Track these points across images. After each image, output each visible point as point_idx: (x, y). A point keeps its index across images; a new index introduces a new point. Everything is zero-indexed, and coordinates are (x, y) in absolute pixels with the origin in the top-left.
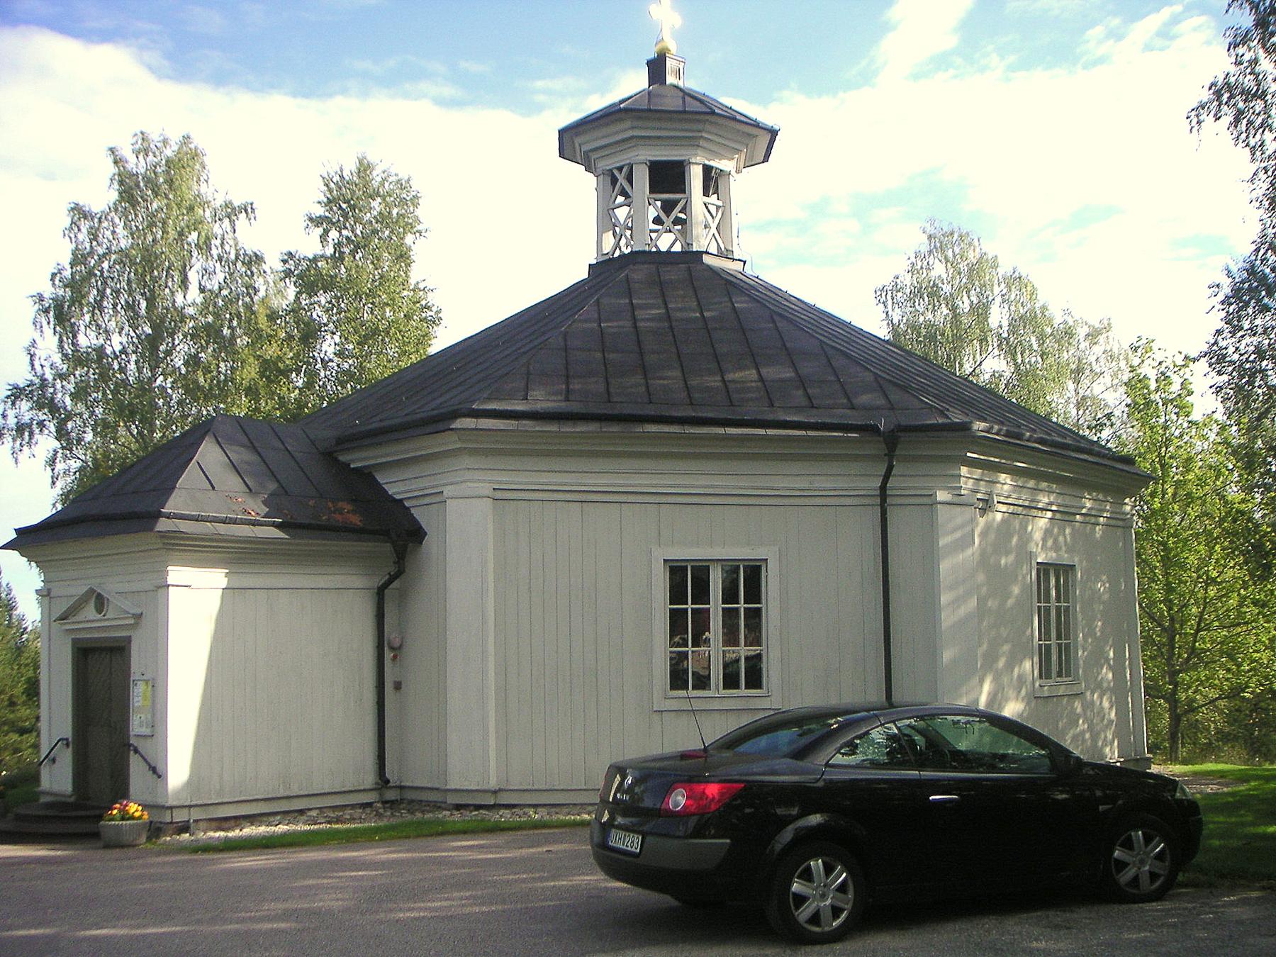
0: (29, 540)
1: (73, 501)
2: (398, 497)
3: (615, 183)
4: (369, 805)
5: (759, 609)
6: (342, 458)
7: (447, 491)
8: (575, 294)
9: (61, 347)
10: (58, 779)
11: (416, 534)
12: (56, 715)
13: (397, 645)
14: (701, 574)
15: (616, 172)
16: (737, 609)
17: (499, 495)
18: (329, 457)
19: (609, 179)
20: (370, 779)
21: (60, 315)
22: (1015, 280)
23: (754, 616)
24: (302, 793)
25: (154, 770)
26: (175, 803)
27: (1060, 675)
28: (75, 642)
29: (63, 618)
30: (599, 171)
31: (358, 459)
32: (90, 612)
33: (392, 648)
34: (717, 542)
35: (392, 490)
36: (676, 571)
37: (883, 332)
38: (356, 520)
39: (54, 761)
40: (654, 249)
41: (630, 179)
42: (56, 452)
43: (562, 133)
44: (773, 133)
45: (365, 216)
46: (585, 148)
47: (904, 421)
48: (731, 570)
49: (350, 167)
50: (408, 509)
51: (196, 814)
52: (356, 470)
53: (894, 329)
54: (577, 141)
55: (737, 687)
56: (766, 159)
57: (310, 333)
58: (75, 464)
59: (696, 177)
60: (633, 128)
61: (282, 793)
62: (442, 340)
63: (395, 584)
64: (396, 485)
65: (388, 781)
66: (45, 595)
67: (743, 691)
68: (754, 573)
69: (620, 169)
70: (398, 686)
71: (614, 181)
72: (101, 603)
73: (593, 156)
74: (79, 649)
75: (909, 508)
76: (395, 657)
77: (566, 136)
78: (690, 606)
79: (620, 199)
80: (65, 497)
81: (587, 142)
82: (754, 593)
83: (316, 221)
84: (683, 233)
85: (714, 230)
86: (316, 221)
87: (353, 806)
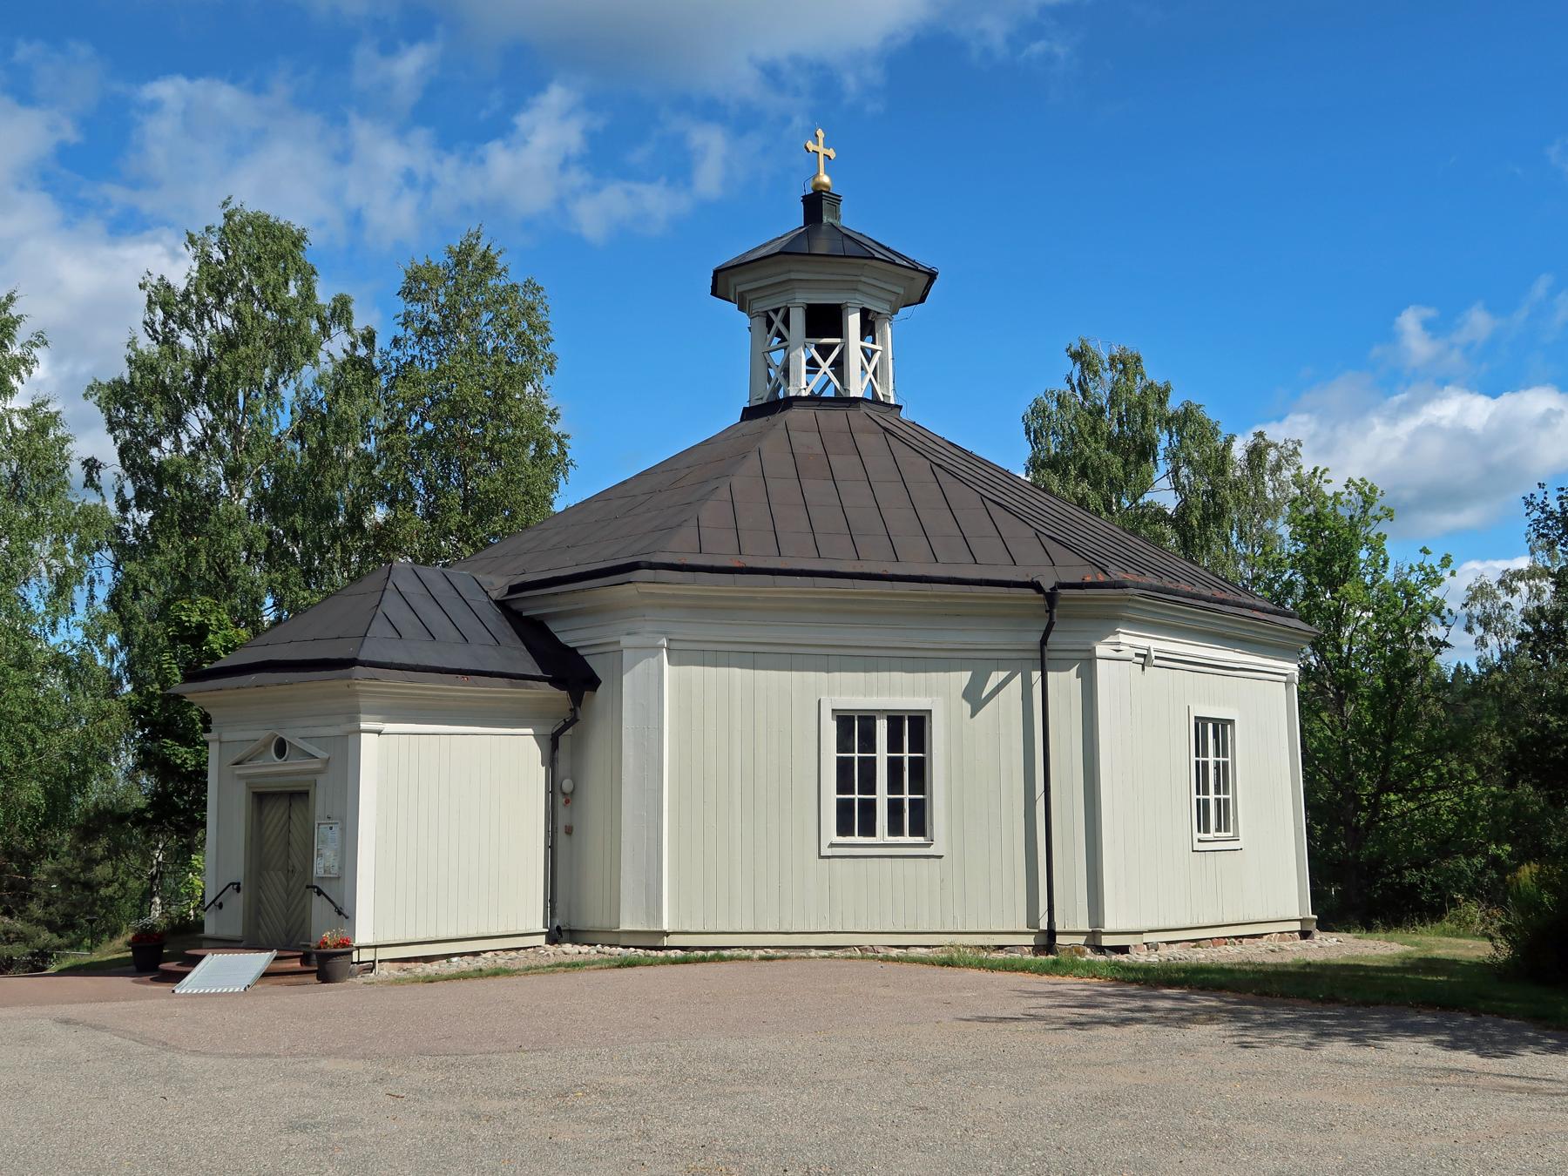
3: (773, 323)
6: (515, 606)
7: (625, 641)
11: (593, 682)
14: (868, 720)
15: (772, 315)
22: (1184, 420)
27: (1218, 830)
28: (249, 786)
35: (562, 638)
38: (1005, 674)
39: (221, 906)
41: (786, 321)
43: (717, 273)
44: (932, 276)
46: (740, 289)
48: (895, 721)
50: (582, 657)
55: (902, 834)
56: (922, 300)
59: (854, 321)
63: (569, 731)
64: (569, 635)
69: (776, 311)
71: (770, 323)
72: (281, 748)
77: (720, 276)
78: (856, 755)
81: (742, 284)
82: (919, 742)
85: (870, 375)
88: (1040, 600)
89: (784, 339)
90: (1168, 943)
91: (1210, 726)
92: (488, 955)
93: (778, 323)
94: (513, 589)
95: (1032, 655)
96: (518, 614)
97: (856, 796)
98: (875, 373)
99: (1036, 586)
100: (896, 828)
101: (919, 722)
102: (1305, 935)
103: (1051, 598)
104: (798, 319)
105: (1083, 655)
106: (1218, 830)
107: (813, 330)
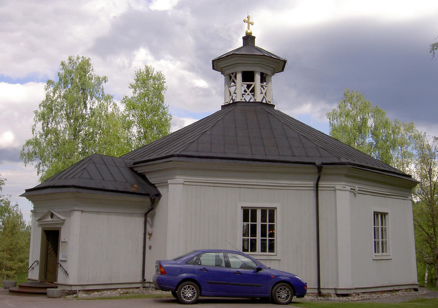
0: (30, 193)
1: (45, 181)
2: (153, 183)
3: (231, 79)
4: (138, 288)
5: (274, 225)
6: (135, 169)
7: (169, 181)
8: (217, 114)
9: (43, 128)
10: (34, 274)
11: (159, 195)
12: (35, 253)
13: (150, 233)
14: (254, 211)
15: (231, 75)
16: (266, 225)
17: (186, 183)
18: (131, 169)
19: (229, 77)
20: (140, 279)
21: (43, 117)
23: (272, 227)
24: (116, 282)
25: (66, 272)
26: (73, 284)
28: (42, 228)
29: (39, 220)
30: (226, 74)
31: (140, 170)
32: (49, 219)
33: (149, 234)
34: (259, 200)
36: (246, 211)
37: (326, 130)
39: (33, 268)
40: (244, 101)
42: (40, 164)
43: (213, 61)
44: (285, 62)
45: (150, 87)
46: (221, 66)
47: (325, 162)
48: (264, 211)
49: (143, 69)
51: (77, 288)
52: (139, 173)
53: (334, 129)
54: (219, 64)
55: (265, 251)
56: (283, 70)
57: (129, 125)
58: (46, 169)
59: (258, 77)
60: (236, 60)
61: (109, 282)
62: (173, 129)
65: (145, 280)
66: (34, 212)
67: (268, 253)
68: (272, 212)
69: (233, 74)
70: (150, 248)
71: (230, 78)
72: (52, 216)
73: (224, 69)
74: (44, 231)
75: (217, 187)
76: (149, 237)
77: (214, 62)
79: (233, 84)
80: (41, 179)
81: (222, 64)
82: (272, 220)
83: (132, 86)
84: (254, 95)
86: (132, 86)
87: (133, 288)
88: (316, 170)
89: (235, 83)
90: (363, 293)
91: (379, 216)
92: (119, 290)
93: (233, 78)
94: (135, 164)
95: (312, 188)
96: (136, 172)
97: (250, 238)
98: (265, 94)
99: (314, 164)
100: (263, 249)
101: (269, 214)
102: (416, 290)
103: (320, 169)
104: (239, 77)
105: (333, 189)
106: (383, 252)
107: (244, 80)
